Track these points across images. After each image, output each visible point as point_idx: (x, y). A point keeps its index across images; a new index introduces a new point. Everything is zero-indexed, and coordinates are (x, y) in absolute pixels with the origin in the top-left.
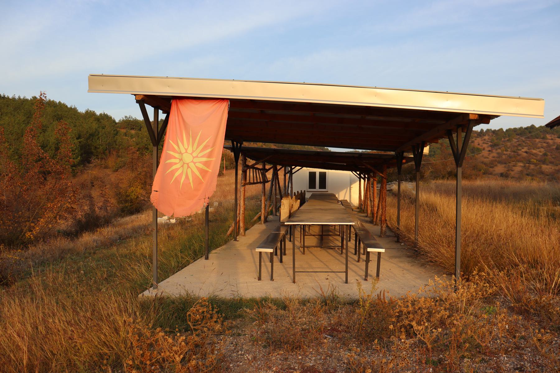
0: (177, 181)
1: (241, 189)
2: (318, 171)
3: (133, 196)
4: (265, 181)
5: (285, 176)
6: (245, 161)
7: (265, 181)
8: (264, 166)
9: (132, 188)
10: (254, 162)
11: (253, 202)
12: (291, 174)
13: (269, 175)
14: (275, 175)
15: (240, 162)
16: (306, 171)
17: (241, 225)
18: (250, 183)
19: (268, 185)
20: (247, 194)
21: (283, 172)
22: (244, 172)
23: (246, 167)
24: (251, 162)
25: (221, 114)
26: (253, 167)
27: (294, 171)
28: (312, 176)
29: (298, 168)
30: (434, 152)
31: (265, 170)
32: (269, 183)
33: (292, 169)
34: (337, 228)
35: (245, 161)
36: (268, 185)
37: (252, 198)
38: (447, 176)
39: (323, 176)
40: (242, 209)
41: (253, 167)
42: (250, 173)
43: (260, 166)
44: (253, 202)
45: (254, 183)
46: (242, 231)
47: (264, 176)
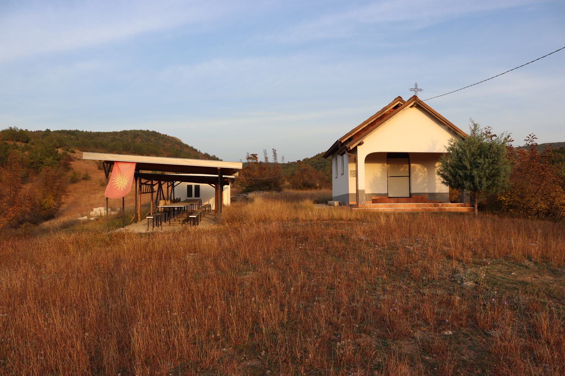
0: (117, 188)
1: (138, 196)
2: (193, 184)
3: (47, 206)
4: (152, 192)
5: (168, 188)
6: (140, 180)
7: (152, 192)
8: (152, 182)
9: (46, 200)
10: (146, 181)
11: (146, 208)
12: (173, 186)
13: (156, 188)
14: (160, 187)
15: (138, 181)
16: (185, 184)
17: (139, 215)
18: (144, 193)
19: (155, 195)
20: (143, 203)
21: (167, 186)
22: (140, 187)
23: (141, 184)
24: (143, 181)
25: (134, 167)
26: (145, 184)
27: (175, 184)
28: (189, 188)
29: (178, 182)
30: (325, 163)
31: (152, 185)
32: (156, 193)
33: (174, 183)
34: (176, 209)
35: (140, 180)
36: (155, 195)
37: (145, 206)
38: (302, 187)
39: (197, 188)
40: (139, 207)
41: (145, 184)
42: (144, 187)
43: (150, 183)
44: (146, 208)
45: (146, 193)
46: (139, 219)
47: (152, 189)
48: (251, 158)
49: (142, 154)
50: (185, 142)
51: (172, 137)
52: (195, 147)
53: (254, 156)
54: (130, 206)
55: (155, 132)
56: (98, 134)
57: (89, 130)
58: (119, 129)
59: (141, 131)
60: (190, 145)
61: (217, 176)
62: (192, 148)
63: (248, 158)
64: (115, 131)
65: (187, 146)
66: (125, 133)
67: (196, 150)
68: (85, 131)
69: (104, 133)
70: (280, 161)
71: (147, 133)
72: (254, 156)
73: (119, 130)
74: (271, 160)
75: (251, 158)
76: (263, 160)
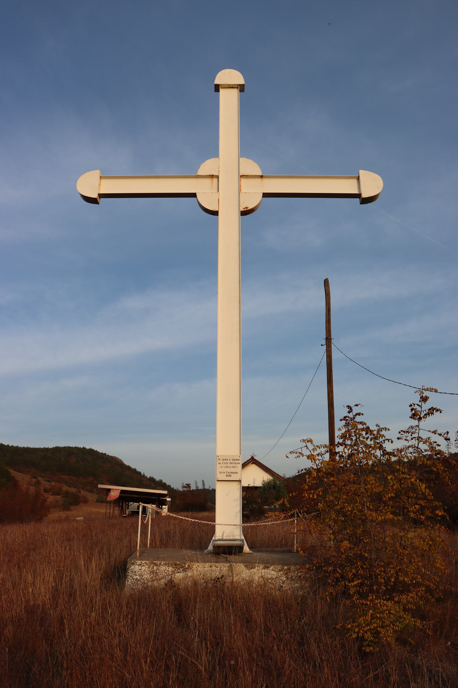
27: (130, 504)
48: (185, 487)
49: (123, 486)
50: (127, 463)
51: (112, 457)
52: (138, 469)
53: (188, 486)
54: (428, 416)
55: (93, 450)
56: (27, 450)
57: (15, 445)
58: (51, 445)
59: (76, 448)
60: (133, 467)
61: (100, 486)
62: (135, 470)
63: (184, 487)
64: (47, 447)
65: (129, 468)
66: (57, 450)
67: (139, 473)
68: (10, 445)
69: (33, 449)
70: (207, 487)
71: (84, 450)
72: (188, 486)
73: (51, 447)
74: (201, 487)
75: (185, 487)
76: (195, 488)
